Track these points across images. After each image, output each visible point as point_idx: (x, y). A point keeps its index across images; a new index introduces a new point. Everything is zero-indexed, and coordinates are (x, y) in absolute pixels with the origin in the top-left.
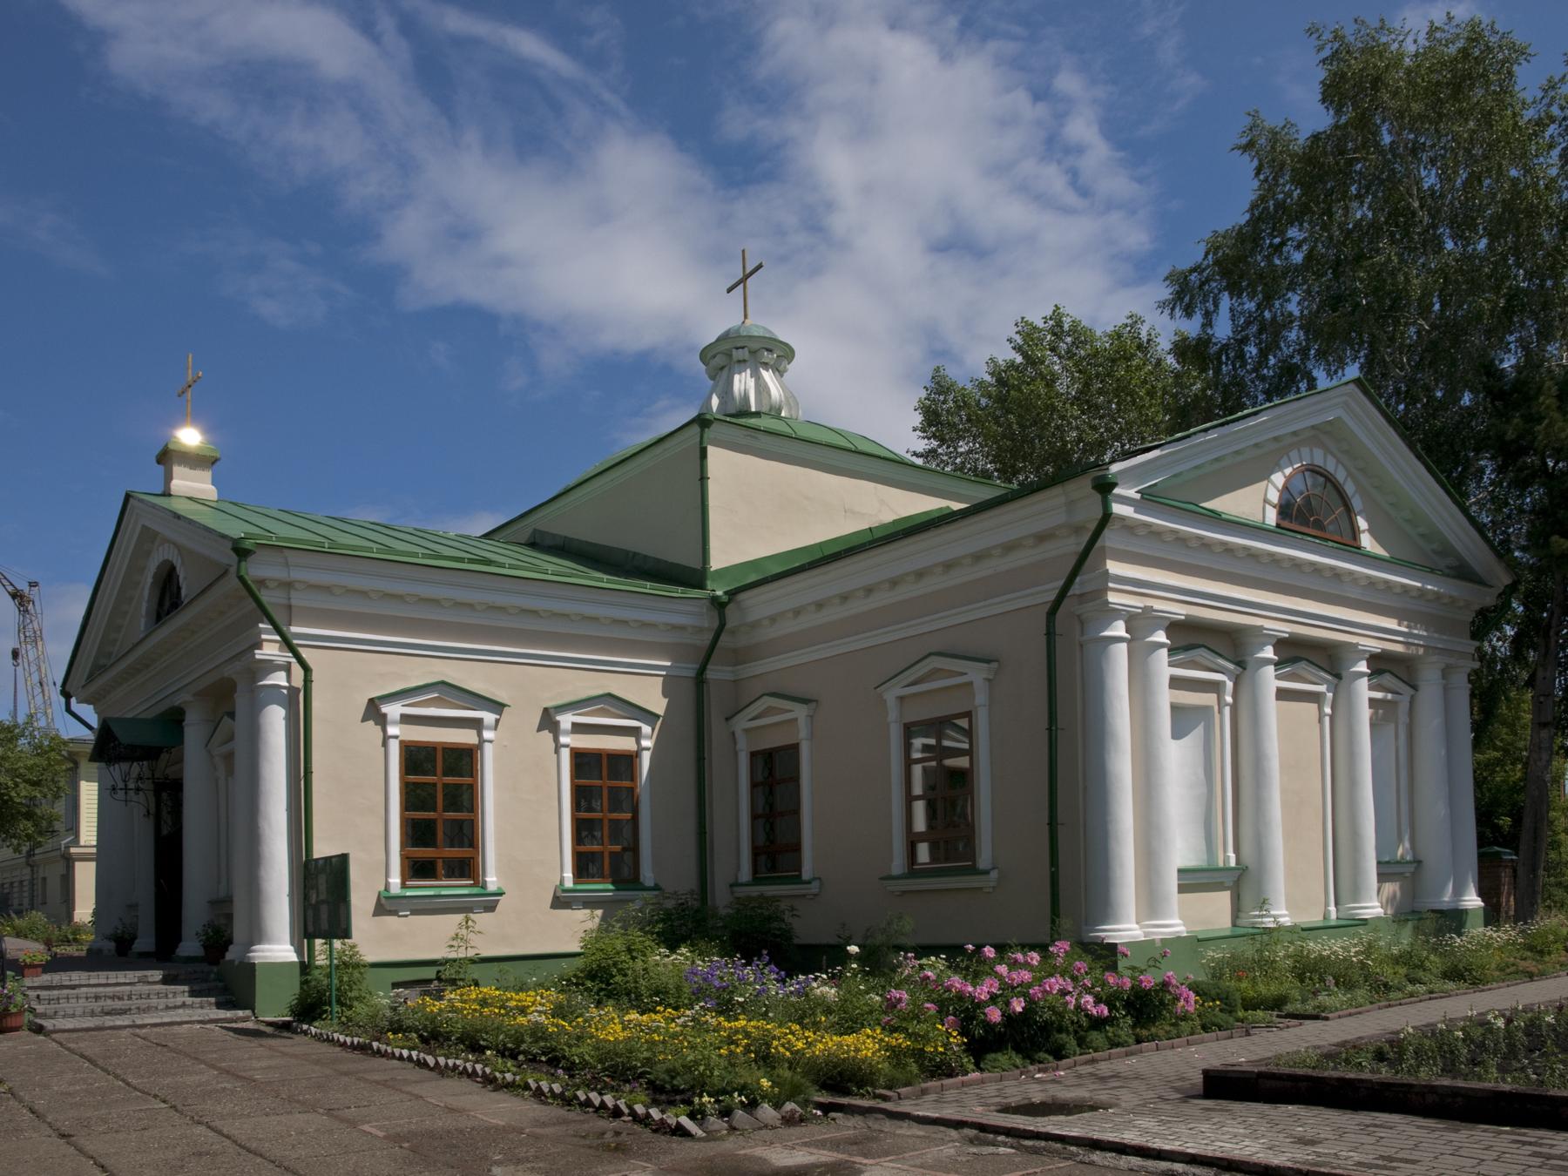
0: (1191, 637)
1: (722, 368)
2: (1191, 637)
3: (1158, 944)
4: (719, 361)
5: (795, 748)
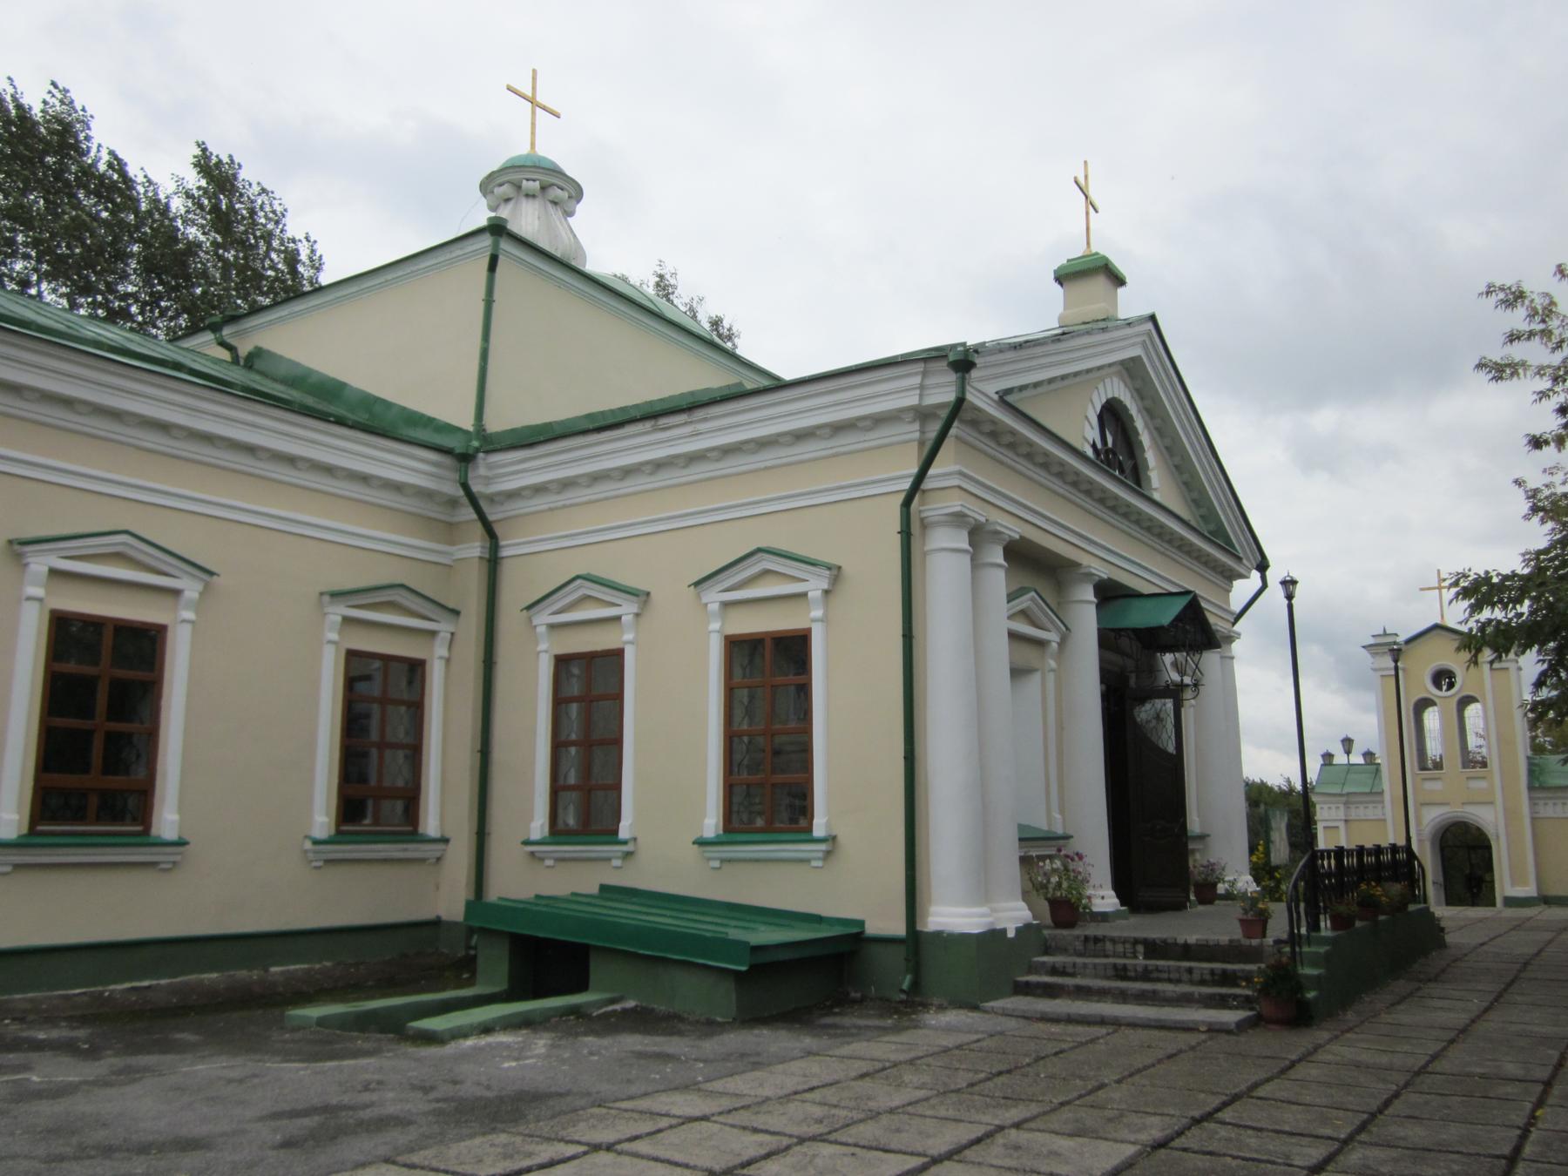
0: (1028, 560)
1: (507, 200)
2: (1028, 560)
3: (1011, 934)
4: (506, 190)
5: (618, 654)
